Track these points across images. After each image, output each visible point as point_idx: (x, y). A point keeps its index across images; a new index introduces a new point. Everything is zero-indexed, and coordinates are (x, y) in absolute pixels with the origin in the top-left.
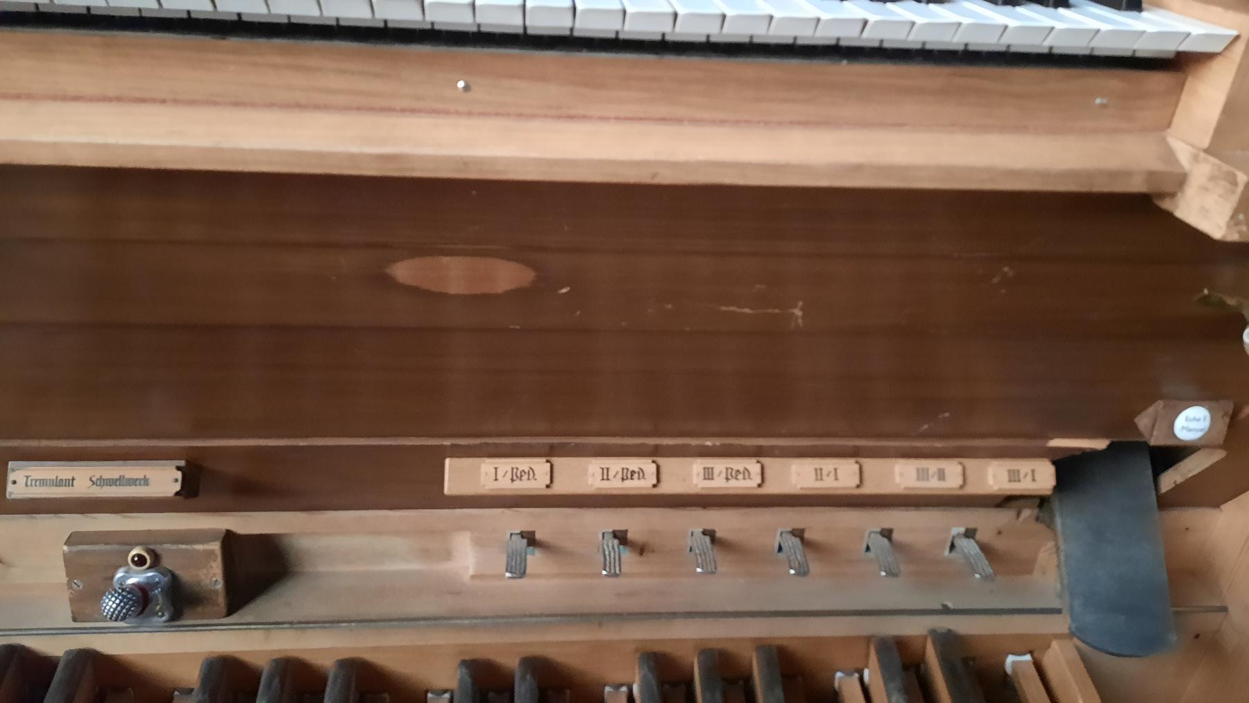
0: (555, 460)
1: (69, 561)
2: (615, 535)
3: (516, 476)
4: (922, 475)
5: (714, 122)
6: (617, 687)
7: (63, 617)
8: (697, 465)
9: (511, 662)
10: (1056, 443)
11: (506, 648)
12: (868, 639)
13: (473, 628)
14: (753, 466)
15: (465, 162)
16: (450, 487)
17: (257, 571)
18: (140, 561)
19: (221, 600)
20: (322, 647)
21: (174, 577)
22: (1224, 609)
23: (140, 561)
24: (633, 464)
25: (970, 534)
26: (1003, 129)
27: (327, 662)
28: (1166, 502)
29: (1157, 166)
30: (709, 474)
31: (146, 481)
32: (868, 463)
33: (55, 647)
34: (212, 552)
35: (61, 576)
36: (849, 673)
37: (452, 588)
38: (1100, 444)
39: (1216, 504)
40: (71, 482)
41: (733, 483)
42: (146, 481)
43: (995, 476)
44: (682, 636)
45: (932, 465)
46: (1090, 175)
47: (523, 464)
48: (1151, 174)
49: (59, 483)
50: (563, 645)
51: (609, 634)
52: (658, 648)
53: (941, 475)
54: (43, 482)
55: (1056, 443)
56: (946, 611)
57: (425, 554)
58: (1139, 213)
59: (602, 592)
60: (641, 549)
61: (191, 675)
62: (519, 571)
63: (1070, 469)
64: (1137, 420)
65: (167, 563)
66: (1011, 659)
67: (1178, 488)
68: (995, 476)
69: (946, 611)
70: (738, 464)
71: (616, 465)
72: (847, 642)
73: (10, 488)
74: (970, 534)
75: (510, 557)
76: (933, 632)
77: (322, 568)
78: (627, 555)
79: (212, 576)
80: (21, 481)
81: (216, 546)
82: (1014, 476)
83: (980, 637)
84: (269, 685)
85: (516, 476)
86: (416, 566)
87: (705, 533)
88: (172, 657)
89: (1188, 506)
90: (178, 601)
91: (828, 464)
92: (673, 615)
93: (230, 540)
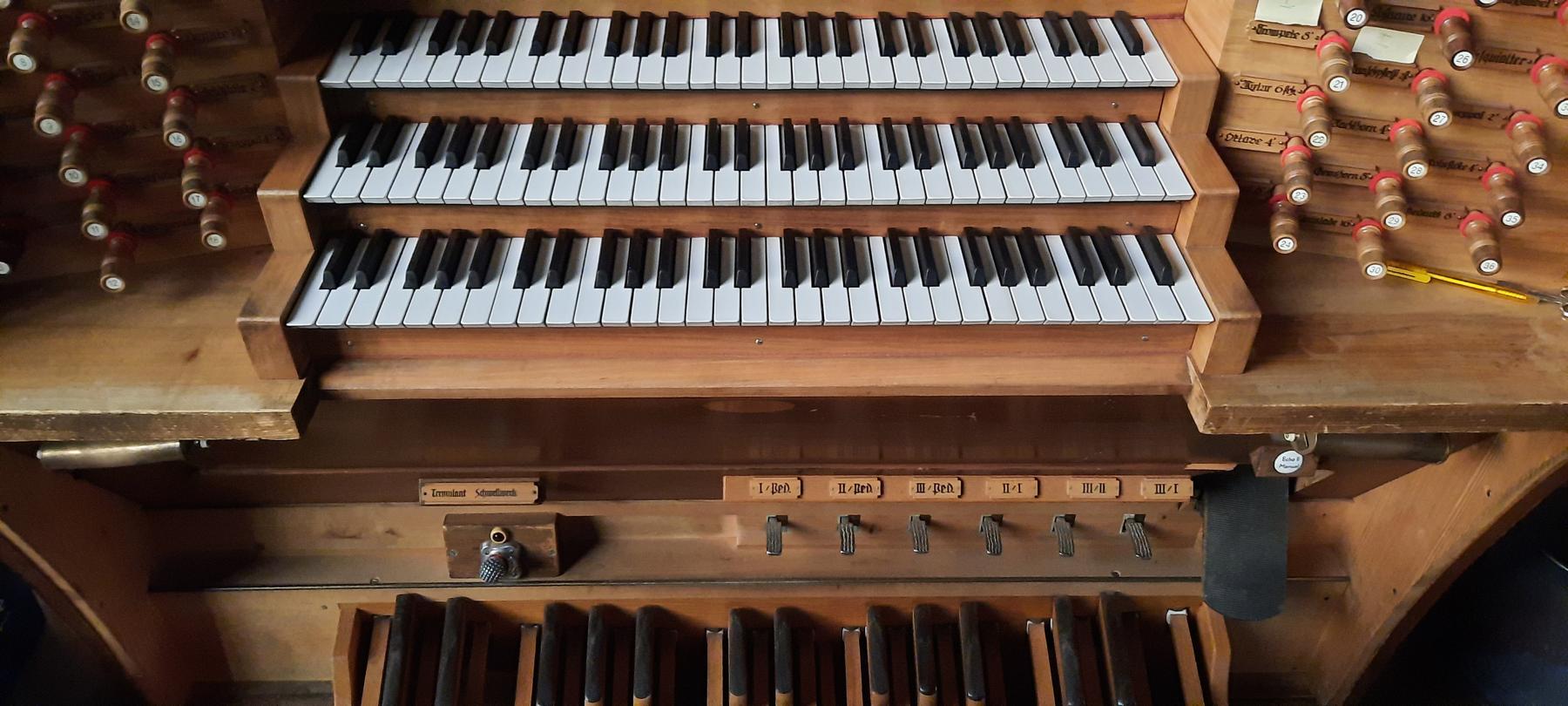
0: (805, 478)
1: (447, 537)
5: (907, 356)
6: (852, 629)
7: (443, 574)
8: (834, 482)
9: (772, 611)
10: (1190, 467)
11: (767, 602)
12: (1052, 598)
13: (742, 587)
15: (761, 390)
17: (580, 541)
18: (499, 537)
19: (556, 564)
20: (631, 599)
21: (522, 548)
22: (1347, 579)
23: (499, 537)
27: (634, 609)
30: (921, 488)
31: (513, 493)
33: (441, 596)
34: (548, 532)
35: (441, 543)
36: (1037, 622)
37: (724, 556)
38: (1229, 467)
39: (1350, 498)
40: (463, 493)
41: (939, 495)
42: (513, 493)
44: (904, 596)
46: (1131, 387)
48: (1170, 387)
49: (455, 494)
50: (810, 599)
51: (845, 593)
52: (884, 603)
53: (1103, 489)
54: (445, 493)
55: (1190, 467)
56: (1116, 578)
57: (701, 528)
59: (840, 564)
60: (871, 529)
61: (539, 616)
62: (775, 547)
63: (1204, 483)
65: (517, 538)
66: (1170, 612)
67: (1306, 489)
69: (1116, 578)
72: (1040, 600)
75: (769, 538)
76: (1104, 594)
77: (624, 537)
78: (859, 534)
79: (550, 547)
80: (430, 493)
81: (552, 527)
83: (1143, 598)
84: (595, 626)
86: (695, 536)
87: (921, 518)
88: (522, 603)
90: (522, 565)
92: (894, 580)
93: (560, 520)
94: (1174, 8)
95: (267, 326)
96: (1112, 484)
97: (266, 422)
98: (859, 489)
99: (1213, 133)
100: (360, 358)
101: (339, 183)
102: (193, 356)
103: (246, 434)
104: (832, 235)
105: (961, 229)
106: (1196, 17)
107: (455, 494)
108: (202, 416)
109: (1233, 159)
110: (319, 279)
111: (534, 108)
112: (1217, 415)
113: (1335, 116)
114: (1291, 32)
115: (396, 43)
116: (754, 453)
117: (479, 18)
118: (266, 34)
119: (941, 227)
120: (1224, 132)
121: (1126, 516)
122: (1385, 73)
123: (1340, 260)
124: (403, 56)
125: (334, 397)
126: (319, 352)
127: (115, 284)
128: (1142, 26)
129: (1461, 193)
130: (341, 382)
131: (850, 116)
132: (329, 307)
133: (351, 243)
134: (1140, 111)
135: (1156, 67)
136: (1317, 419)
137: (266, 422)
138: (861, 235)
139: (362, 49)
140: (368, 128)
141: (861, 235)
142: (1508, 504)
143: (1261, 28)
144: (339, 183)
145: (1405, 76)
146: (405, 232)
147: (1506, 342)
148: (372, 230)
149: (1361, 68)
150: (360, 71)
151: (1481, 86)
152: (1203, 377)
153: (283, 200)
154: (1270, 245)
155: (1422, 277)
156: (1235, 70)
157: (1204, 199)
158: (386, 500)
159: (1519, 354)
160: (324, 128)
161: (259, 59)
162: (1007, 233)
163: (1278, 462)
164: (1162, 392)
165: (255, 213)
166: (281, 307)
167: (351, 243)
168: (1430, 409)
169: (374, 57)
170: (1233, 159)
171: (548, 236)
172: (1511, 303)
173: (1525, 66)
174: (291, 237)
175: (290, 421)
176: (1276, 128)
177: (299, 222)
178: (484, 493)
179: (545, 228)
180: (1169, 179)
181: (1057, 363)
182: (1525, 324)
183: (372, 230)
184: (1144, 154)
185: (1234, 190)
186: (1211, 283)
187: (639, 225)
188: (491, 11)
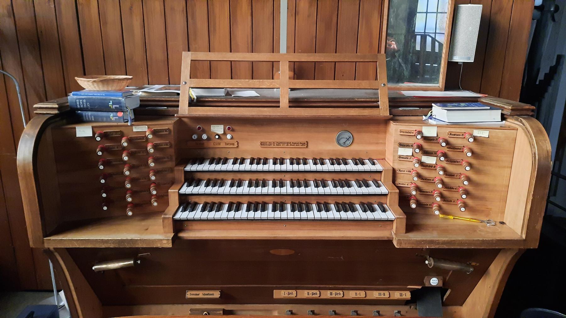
2: (311, 311)
3: (289, 294)
4: (380, 294)
8: (306, 292)
14: (341, 292)
15: (286, 237)
16: (275, 296)
24: (314, 291)
25: (399, 312)
26: (366, 230)
28: (444, 304)
29: (389, 236)
30: (331, 294)
32: (368, 292)
40: (198, 295)
42: (213, 295)
43: (396, 295)
45: (382, 292)
46: (379, 237)
47: (290, 291)
49: (196, 295)
53: (384, 295)
58: (389, 242)
64: (275, 291)
68: (396, 295)
70: (338, 292)
71: (311, 292)
73: (187, 296)
74: (399, 312)
81: (222, 312)
82: (401, 295)
85: (289, 294)
89: (147, 304)
91: (358, 292)
94: (383, 157)
95: (168, 218)
96: (387, 293)
97: (165, 242)
98: (313, 294)
99: (394, 181)
100: (188, 230)
101: (186, 190)
102: (147, 229)
103: (159, 246)
104: (303, 204)
105: (334, 202)
106: (388, 159)
107: (196, 295)
108: (150, 240)
109: (398, 187)
110: (181, 209)
111: (232, 176)
112: (399, 242)
113: (419, 176)
114: (407, 157)
115: (201, 162)
116: (283, 252)
117: (220, 159)
118: (174, 159)
119: (329, 202)
120: (397, 182)
121: (395, 312)
122: (430, 166)
123: (431, 215)
124: (203, 165)
125: (180, 238)
126: (179, 226)
127: (130, 213)
128: (375, 161)
129: (455, 196)
130: (182, 235)
131: (307, 179)
132: (182, 215)
133: (186, 202)
134: (377, 178)
135: (378, 167)
136: (424, 244)
137: (165, 242)
138: (310, 204)
139: (193, 163)
140: (192, 179)
141: (310, 204)
142: (496, 287)
143: (400, 157)
144: (186, 190)
145: (435, 167)
146: (199, 202)
147: (473, 229)
148: (192, 202)
149: (422, 164)
150: (190, 168)
151: (451, 168)
152: (395, 234)
153: (174, 192)
154: (413, 210)
155: (451, 217)
156: (396, 167)
157: (391, 193)
158: (173, 303)
159: (475, 231)
160: (183, 180)
161: (170, 164)
162: (346, 203)
163: (431, 281)
164: (386, 239)
165: (167, 195)
166: (173, 213)
167: (186, 202)
168: (452, 241)
169: (196, 165)
170: (398, 187)
171: (234, 204)
172: (474, 223)
173: (460, 163)
174: (174, 200)
175: (171, 241)
176: (408, 181)
177: (177, 198)
178: (204, 295)
179: (233, 201)
180: (383, 190)
181: (359, 232)
182: (477, 226)
183: (192, 202)
184: (377, 185)
185: (398, 191)
186: (395, 212)
187: (256, 201)
188: (222, 157)
